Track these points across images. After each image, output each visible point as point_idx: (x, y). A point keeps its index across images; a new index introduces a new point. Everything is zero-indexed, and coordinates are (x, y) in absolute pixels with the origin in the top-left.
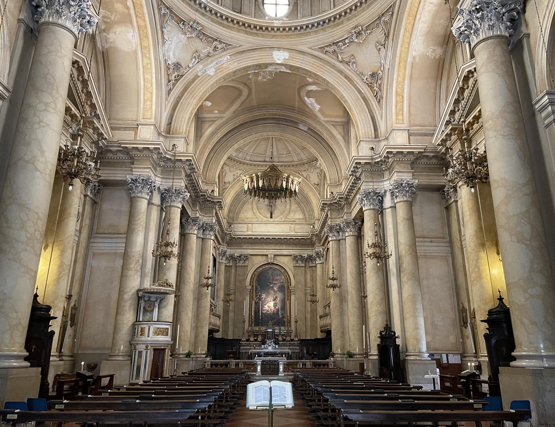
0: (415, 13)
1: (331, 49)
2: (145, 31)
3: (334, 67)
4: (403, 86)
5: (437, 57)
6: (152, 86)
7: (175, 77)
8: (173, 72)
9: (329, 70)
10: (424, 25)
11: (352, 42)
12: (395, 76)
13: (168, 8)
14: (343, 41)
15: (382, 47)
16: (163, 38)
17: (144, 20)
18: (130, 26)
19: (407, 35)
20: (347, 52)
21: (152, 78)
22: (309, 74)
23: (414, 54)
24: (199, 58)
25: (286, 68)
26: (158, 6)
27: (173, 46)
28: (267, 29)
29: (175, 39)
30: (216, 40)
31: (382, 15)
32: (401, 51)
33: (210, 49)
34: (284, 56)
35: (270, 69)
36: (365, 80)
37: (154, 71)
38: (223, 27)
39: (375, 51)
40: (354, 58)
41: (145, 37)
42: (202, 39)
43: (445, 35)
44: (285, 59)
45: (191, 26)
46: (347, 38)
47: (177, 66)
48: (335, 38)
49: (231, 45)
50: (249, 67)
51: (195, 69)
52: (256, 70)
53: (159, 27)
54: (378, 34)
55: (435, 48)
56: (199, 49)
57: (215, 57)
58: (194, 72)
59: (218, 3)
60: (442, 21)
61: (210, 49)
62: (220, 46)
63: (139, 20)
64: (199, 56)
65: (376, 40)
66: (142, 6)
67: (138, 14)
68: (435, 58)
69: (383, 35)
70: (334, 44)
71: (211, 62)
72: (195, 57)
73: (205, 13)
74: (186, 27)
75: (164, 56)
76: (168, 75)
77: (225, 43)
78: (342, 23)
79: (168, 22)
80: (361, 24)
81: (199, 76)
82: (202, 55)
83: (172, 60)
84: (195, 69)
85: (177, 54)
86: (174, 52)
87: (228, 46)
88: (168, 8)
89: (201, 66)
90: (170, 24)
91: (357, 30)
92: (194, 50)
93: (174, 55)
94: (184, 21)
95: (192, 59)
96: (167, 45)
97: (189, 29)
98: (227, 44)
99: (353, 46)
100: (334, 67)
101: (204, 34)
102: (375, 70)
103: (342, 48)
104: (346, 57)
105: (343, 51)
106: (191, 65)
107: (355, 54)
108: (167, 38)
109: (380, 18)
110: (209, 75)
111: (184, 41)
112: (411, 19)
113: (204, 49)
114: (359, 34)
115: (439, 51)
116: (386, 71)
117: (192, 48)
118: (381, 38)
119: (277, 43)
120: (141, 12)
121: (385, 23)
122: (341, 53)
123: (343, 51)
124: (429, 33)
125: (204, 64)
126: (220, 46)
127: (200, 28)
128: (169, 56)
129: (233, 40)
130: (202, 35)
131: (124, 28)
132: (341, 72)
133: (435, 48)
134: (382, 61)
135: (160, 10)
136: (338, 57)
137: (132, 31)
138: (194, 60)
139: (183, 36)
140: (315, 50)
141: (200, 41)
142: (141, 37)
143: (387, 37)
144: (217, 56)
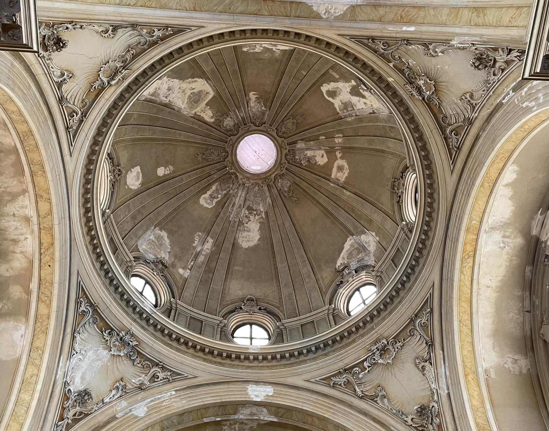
0: (468, 296)
1: (341, 380)
2: (45, 323)
3: (351, 406)
4: (485, 413)
5: (524, 371)
6: (27, 412)
7: (74, 415)
8: (74, 406)
9: (344, 410)
10: (486, 321)
11: (375, 364)
12: (465, 397)
13: (91, 305)
14: (361, 366)
15: (427, 364)
16: (72, 347)
17: (49, 306)
18: (24, 320)
19: (466, 330)
20: (370, 380)
21: (32, 399)
22: (310, 419)
23: (485, 365)
24: (122, 389)
25: (270, 413)
26: (78, 298)
27: (84, 365)
28: (238, 358)
29: (90, 354)
30: (157, 365)
31: (416, 316)
32: (463, 357)
33: (145, 379)
34: (265, 391)
35: (242, 415)
36: (410, 422)
37: (39, 387)
38: (171, 348)
39: (416, 373)
40: (383, 389)
41: (43, 332)
42: (134, 361)
43: (525, 337)
44: (267, 396)
45: (121, 339)
46: (365, 360)
47: (84, 396)
48: (346, 362)
49: (180, 374)
50: (206, 408)
51: (112, 407)
52: (217, 416)
53: (69, 330)
54: (415, 347)
55: (516, 357)
56: (127, 376)
57: (151, 391)
58: (110, 411)
59: (169, 317)
60: (511, 314)
61: (145, 379)
62: (161, 375)
63: (42, 306)
64: (125, 387)
65: (414, 355)
66: (52, 283)
67: (42, 296)
68: (521, 372)
69: (424, 345)
70: (345, 370)
71: (143, 399)
72: (117, 388)
73: (146, 327)
74: (113, 339)
75: (65, 375)
76: (63, 409)
77: (171, 371)
78: (354, 341)
79: (87, 326)
80: (386, 334)
81: (117, 418)
82: (129, 386)
83: (77, 386)
84: (112, 407)
85: (88, 378)
86: (84, 374)
87: (175, 375)
88: (91, 305)
89: (124, 404)
90: (89, 330)
91: (379, 345)
92: (118, 377)
93: (83, 378)
94: (112, 330)
95: (111, 391)
96: (74, 360)
97: (117, 343)
98: (174, 372)
99: (377, 371)
100: (351, 406)
101: (138, 352)
102: (425, 402)
103: (361, 376)
104: (369, 389)
105: (363, 381)
106: (107, 400)
107: (384, 384)
108: (78, 350)
109: (412, 321)
110: (137, 417)
111: (105, 360)
112: (466, 305)
113: (134, 375)
114: (384, 351)
115: (524, 363)
116: (445, 399)
117: (116, 372)
118: (422, 349)
119: (254, 375)
120: (48, 294)
121: (424, 326)
122: (359, 385)
123: (363, 381)
124: (498, 334)
125: (130, 401)
126: (161, 375)
127: (135, 343)
128: (73, 378)
129: (184, 367)
130: (136, 354)
131: (12, 323)
132: (365, 414)
133: (516, 357)
134: (433, 386)
135: (78, 303)
136: (355, 391)
137: (23, 327)
138: (114, 392)
139: (105, 352)
140: (316, 382)
141: (130, 363)
142: (36, 332)
143: (431, 345)
144: (155, 391)
